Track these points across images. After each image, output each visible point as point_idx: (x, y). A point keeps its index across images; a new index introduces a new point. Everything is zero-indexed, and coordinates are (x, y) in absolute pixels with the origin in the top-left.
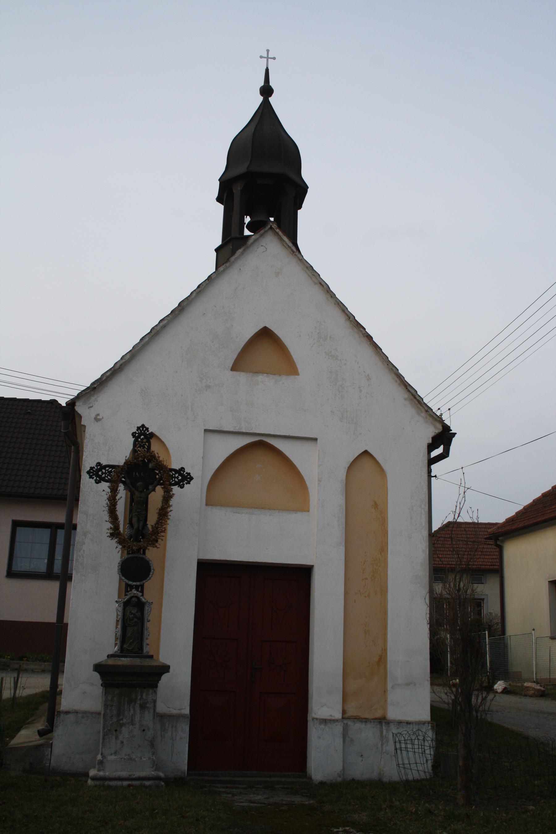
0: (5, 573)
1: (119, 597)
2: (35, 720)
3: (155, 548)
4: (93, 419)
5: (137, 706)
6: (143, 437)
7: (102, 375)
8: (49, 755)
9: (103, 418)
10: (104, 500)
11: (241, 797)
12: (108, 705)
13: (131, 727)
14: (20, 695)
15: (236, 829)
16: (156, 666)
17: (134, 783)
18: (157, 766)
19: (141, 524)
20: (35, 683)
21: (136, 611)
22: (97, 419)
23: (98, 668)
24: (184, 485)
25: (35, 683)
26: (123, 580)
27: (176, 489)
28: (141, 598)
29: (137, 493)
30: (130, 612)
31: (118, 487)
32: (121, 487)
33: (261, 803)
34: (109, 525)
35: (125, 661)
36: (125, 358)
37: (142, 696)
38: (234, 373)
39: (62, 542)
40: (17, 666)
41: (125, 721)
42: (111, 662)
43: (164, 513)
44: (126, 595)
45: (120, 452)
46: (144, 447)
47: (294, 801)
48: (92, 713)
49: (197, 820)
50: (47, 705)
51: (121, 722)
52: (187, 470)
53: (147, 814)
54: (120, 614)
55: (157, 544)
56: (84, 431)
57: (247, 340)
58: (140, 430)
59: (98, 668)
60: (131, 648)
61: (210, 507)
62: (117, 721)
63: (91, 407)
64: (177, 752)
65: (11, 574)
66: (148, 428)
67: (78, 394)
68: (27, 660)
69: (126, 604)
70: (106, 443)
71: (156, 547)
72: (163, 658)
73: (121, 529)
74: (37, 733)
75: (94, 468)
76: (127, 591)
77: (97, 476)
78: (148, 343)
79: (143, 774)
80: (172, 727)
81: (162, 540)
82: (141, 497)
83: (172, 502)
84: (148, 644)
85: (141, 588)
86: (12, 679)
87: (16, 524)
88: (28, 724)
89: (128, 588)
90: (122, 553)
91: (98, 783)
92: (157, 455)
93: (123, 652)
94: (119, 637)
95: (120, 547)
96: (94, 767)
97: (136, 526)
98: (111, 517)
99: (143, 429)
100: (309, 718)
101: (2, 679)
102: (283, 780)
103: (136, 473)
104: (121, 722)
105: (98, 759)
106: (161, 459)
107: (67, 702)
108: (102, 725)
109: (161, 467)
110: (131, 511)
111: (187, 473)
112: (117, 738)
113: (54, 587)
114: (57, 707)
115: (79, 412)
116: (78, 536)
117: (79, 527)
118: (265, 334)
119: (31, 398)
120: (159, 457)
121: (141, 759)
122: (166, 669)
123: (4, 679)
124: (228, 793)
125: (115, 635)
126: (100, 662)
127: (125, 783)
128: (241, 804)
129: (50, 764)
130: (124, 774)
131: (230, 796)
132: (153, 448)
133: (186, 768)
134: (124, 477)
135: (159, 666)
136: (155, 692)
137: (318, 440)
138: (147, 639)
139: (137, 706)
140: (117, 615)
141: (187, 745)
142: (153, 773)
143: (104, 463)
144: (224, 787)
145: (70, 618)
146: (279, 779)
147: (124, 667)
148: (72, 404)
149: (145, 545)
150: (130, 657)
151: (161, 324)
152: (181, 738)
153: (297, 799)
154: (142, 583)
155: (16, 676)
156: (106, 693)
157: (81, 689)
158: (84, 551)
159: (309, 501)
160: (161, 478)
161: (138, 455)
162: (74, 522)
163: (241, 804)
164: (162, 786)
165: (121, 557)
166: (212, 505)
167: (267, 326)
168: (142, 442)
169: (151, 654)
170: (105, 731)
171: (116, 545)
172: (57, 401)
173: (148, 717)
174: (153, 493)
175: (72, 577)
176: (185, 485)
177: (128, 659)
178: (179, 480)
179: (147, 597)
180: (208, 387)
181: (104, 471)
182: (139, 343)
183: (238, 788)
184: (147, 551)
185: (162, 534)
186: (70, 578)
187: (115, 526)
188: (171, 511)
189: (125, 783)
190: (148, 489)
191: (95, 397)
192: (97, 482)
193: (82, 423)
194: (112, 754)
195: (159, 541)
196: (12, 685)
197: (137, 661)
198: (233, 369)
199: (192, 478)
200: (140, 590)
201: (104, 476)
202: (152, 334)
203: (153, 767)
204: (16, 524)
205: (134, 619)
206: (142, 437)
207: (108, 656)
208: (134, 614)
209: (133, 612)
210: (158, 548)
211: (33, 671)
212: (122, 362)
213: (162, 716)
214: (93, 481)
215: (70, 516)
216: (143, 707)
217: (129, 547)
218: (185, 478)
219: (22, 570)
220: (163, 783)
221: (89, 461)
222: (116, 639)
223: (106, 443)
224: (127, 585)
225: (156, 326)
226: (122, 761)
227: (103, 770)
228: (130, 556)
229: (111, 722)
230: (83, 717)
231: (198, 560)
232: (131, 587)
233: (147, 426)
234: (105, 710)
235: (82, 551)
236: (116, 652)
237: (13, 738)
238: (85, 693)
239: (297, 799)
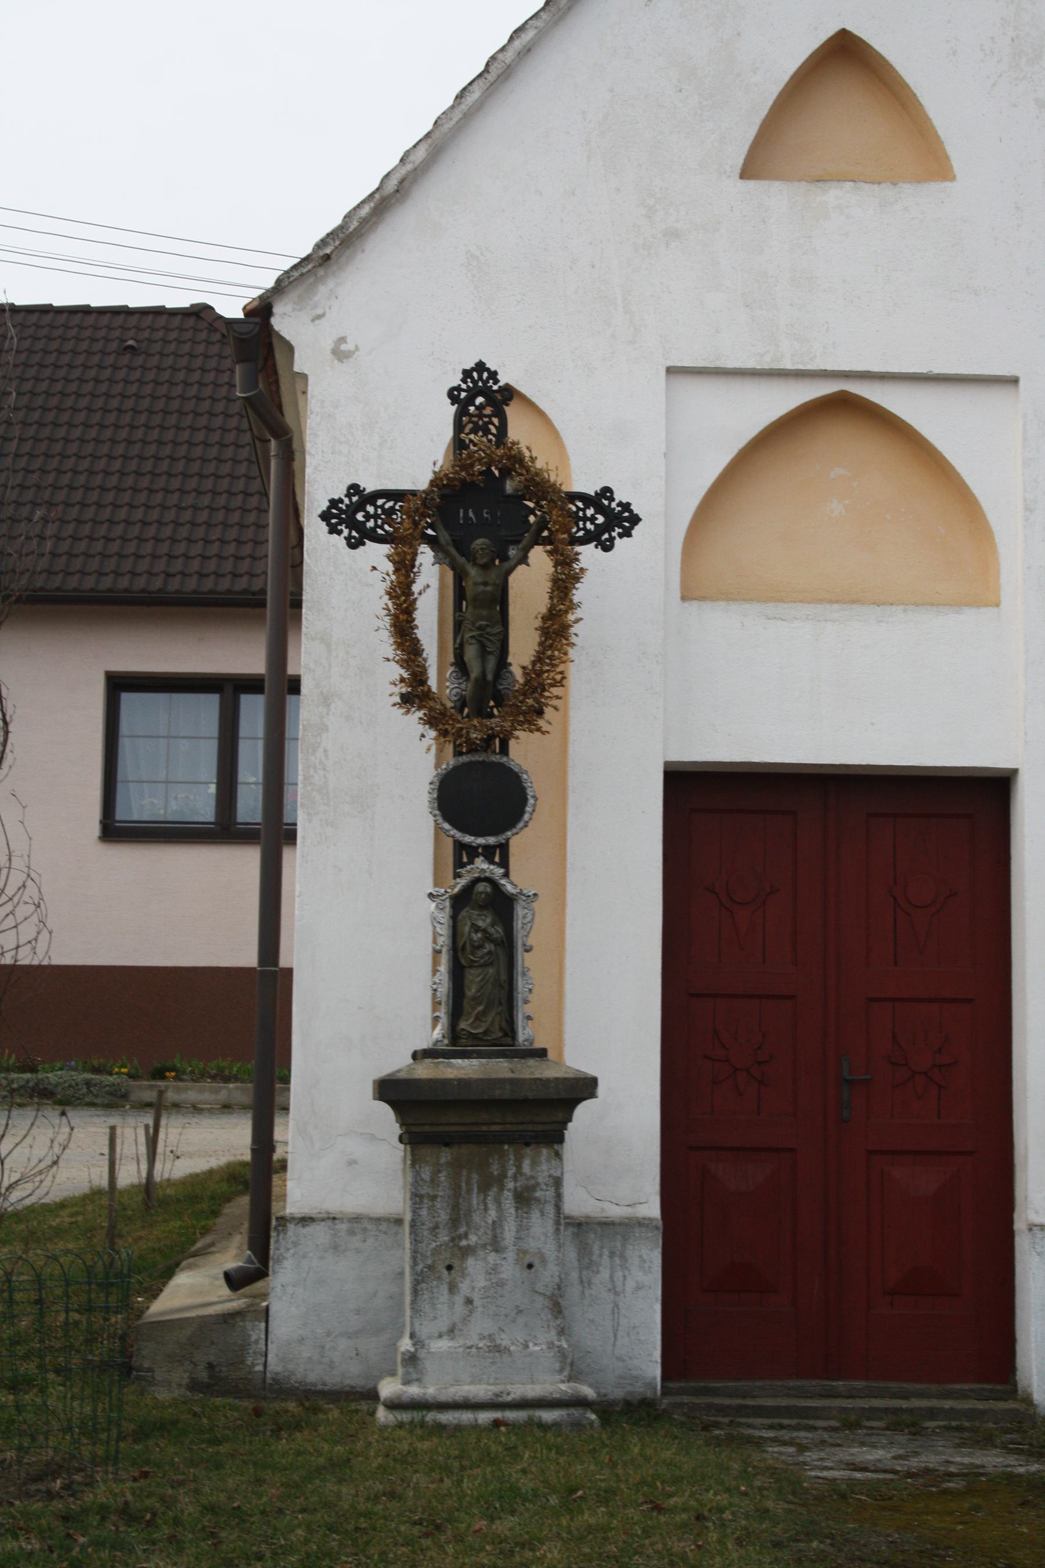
0: (96, 829)
1: (437, 883)
2: (212, 1244)
3: (537, 734)
4: (328, 352)
5: (508, 1195)
6: (483, 400)
7: (348, 217)
8: (263, 1342)
9: (357, 348)
10: (376, 599)
11: (822, 1455)
12: (421, 1197)
13: (492, 1258)
14: (166, 1176)
15: (815, 1544)
16: (557, 1079)
17: (511, 1415)
18: (572, 1367)
19: (492, 663)
20: (206, 1142)
21: (489, 920)
22: (340, 354)
23: (390, 1090)
24: (612, 539)
25: (206, 1142)
26: (446, 831)
27: (588, 554)
28: (503, 882)
29: (473, 572)
30: (473, 925)
31: (415, 554)
32: (426, 556)
33: (885, 1471)
34: (397, 671)
35: (464, 1068)
36: (412, 158)
37: (519, 1167)
38: (752, 184)
39: (260, 732)
40: (150, 1096)
41: (473, 1239)
42: (425, 1071)
43: (556, 628)
44: (457, 875)
45: (415, 452)
46: (487, 432)
47: (983, 1467)
48: (378, 1220)
49: (699, 1517)
50: (245, 1201)
51: (464, 1243)
52: (620, 496)
53: (554, 1500)
54: (444, 931)
55: (541, 723)
56: (304, 393)
57: (786, 78)
58: (474, 381)
59: (390, 1090)
60: (480, 1030)
61: (695, 603)
62: (453, 1240)
63: (319, 317)
64: (630, 1328)
65: (113, 831)
66: (495, 373)
67: (279, 281)
68: (178, 1078)
69: (460, 902)
70: (371, 424)
71: (539, 729)
72: (576, 1058)
73: (433, 682)
74: (222, 1282)
75: (341, 501)
76: (459, 864)
77: (353, 524)
78: (479, 106)
79: (533, 1391)
80: (612, 1254)
81: (556, 708)
82: (485, 584)
83: (579, 594)
84: (529, 1018)
85: (501, 854)
86: (141, 1132)
87: (118, 685)
88: (195, 1255)
89: (463, 854)
90: (440, 751)
91: (405, 1416)
92: (527, 454)
93: (458, 1042)
94: (444, 999)
95: (433, 733)
96: (393, 1374)
97: (475, 672)
98: (399, 645)
99: (480, 378)
100: (1019, 1224)
101: (113, 1129)
102: (947, 1404)
103: (466, 513)
104: (464, 1243)
105: (402, 1349)
106: (539, 464)
107: (298, 1192)
108: (408, 1254)
109: (540, 488)
110: (458, 626)
111: (620, 504)
112: (453, 1288)
113: (246, 862)
114: (276, 1209)
115: (285, 333)
116: (307, 711)
117: (307, 686)
118: (845, 55)
119: (133, 303)
120: (533, 459)
121: (527, 1347)
122: (585, 1087)
123: (119, 1131)
124: (785, 1444)
125: (430, 992)
126: (388, 1075)
127: (485, 1417)
128: (825, 1474)
129: (265, 1365)
130: (480, 1391)
131: (791, 1450)
132: (514, 434)
133: (655, 1371)
134: (431, 526)
135: (565, 1079)
136: (558, 1155)
137: (1021, 383)
138: (526, 1002)
139: (508, 1195)
140: (435, 936)
141: (658, 1307)
142: (563, 1387)
143: (370, 486)
144: (771, 1427)
145: (294, 953)
146: (934, 1403)
147: (463, 1083)
148: (261, 311)
149: (507, 725)
150: (480, 1055)
151: (518, 44)
152: (639, 1288)
153: (992, 1460)
154: (501, 838)
155: (151, 1123)
156: (415, 1161)
157: (341, 1151)
158: (325, 751)
159: (998, 572)
160: (542, 525)
161: (470, 456)
162: (291, 670)
163: (825, 1474)
164: (591, 1423)
165: (437, 766)
166: (702, 598)
167: (849, 28)
168: (481, 416)
169: (538, 1045)
170: (419, 1268)
171: (421, 728)
172: (210, 308)
173: (540, 1227)
174: (521, 568)
175: (295, 831)
176: (618, 542)
177: (475, 1062)
178: (597, 526)
179: (521, 877)
180: (673, 234)
181: (370, 509)
182: (452, 107)
183: (815, 1429)
184: (512, 743)
185: (555, 691)
186: (290, 837)
187: (414, 674)
188: (577, 621)
189: (485, 1417)
190: (505, 558)
191: (331, 283)
192: (353, 544)
193: (297, 368)
194: (440, 1336)
195: (548, 711)
196: (143, 1149)
197: (500, 1068)
198: (746, 173)
199: (635, 520)
200: (497, 859)
201: (371, 524)
202: (491, 77)
203: (561, 1371)
204: (118, 685)
205: (485, 948)
206: (480, 400)
207: (415, 1056)
208: (484, 931)
209: (480, 923)
210: (543, 733)
211: (196, 1109)
212: (403, 171)
213: (580, 1225)
214: (339, 541)
215: (278, 654)
216: (524, 1199)
217: (458, 734)
218: (613, 519)
219: (145, 818)
220: (593, 1417)
221: (322, 484)
222: (436, 1004)
223: (371, 424)
224: (460, 847)
225: (503, 49)
226: (471, 1352)
227: (417, 1380)
228: (464, 759)
229: (434, 1244)
230: (351, 1232)
231: (667, 764)
232: (473, 852)
233: (491, 365)
234: (415, 1211)
235: (320, 753)
236: (437, 1041)
237: (155, 1296)
238: (352, 1163)
239: (992, 1460)
